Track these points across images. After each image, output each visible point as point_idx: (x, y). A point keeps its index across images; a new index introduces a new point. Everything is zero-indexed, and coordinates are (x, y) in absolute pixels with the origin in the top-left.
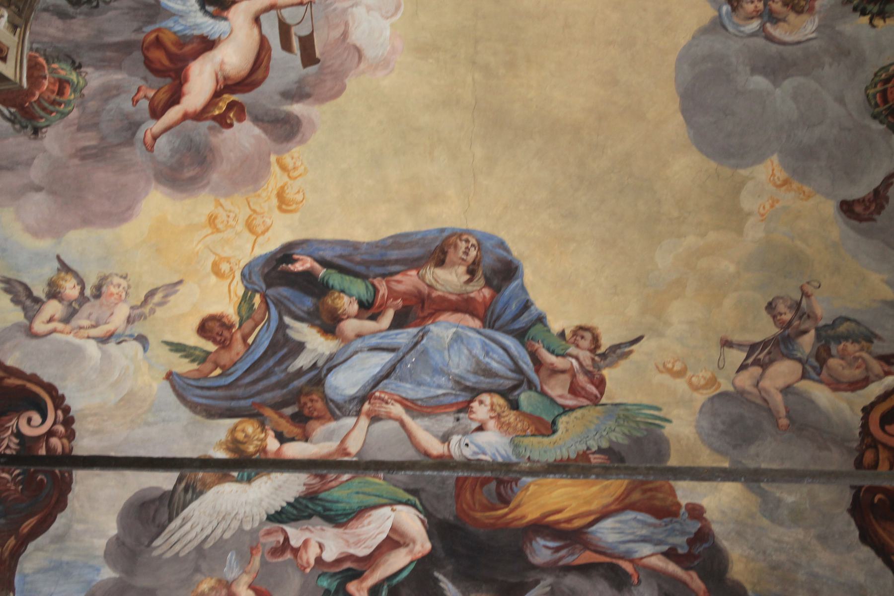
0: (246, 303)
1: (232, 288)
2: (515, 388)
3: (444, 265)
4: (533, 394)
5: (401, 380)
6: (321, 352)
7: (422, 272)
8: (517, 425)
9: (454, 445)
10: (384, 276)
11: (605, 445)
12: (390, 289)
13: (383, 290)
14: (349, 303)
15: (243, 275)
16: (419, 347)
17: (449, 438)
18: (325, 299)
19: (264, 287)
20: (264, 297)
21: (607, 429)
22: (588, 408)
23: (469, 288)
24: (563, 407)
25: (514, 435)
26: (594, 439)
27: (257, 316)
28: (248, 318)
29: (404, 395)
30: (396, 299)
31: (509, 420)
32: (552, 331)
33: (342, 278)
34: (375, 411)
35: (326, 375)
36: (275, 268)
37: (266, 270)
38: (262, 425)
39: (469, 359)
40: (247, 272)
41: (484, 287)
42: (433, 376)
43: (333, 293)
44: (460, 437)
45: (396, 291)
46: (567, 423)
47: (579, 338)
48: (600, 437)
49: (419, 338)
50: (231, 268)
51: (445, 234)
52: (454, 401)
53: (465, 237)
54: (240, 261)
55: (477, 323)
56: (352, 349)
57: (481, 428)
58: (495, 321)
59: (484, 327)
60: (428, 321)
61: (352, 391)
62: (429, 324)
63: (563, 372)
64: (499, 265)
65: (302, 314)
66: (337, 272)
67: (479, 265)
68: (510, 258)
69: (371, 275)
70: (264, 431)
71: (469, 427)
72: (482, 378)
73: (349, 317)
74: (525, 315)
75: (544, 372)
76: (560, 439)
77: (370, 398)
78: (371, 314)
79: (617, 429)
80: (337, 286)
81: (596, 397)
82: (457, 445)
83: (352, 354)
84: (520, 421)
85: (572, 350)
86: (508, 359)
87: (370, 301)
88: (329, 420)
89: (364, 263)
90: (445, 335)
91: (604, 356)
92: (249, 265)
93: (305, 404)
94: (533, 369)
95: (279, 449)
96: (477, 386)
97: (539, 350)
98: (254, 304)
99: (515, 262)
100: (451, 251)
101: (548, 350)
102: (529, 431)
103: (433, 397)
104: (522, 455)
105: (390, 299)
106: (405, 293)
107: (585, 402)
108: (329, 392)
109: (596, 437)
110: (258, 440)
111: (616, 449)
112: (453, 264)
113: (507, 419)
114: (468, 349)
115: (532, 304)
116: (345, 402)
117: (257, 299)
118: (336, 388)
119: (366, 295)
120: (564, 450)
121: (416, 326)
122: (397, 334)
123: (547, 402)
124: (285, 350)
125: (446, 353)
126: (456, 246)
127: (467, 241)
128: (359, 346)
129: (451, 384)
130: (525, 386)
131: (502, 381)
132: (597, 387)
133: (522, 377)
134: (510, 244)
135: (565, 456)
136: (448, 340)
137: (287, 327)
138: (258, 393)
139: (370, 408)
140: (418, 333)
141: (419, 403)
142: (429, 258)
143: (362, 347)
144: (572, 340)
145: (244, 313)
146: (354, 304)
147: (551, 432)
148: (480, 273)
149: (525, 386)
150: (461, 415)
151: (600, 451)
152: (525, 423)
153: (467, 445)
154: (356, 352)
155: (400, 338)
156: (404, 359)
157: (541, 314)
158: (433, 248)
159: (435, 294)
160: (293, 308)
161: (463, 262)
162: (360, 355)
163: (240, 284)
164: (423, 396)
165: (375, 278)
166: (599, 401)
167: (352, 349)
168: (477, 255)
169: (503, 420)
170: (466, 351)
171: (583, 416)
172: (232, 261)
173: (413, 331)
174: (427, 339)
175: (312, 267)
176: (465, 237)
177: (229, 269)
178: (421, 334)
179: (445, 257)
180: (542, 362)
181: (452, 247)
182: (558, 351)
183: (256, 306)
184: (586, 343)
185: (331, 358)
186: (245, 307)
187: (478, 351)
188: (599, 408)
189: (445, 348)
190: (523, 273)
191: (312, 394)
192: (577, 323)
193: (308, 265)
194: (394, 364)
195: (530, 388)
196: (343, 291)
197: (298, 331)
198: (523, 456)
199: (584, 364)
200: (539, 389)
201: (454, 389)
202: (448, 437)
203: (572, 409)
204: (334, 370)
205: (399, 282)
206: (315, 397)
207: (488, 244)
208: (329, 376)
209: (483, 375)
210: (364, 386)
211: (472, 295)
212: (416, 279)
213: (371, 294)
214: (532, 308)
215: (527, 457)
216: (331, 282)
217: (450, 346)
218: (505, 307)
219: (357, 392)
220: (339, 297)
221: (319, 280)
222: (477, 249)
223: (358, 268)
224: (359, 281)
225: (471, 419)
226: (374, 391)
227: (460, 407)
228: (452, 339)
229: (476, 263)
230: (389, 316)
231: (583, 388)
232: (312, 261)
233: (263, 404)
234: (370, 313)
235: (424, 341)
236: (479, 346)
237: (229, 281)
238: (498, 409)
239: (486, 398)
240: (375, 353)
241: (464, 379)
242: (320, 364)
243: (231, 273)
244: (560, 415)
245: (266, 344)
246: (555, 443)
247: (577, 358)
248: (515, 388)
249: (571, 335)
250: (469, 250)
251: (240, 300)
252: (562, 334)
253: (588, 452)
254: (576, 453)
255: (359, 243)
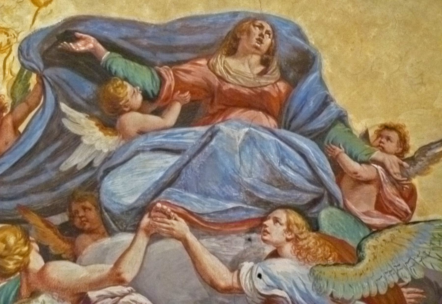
0: (21, 83)
1: (7, 63)
2: (315, 202)
3: (237, 54)
4: (334, 210)
5: (186, 189)
6: (99, 149)
7: (213, 61)
8: (317, 250)
9: (246, 273)
10: (171, 64)
11: (419, 275)
12: (177, 79)
13: (170, 81)
14: (132, 93)
15: (20, 50)
16: (207, 149)
17: (240, 265)
18: (108, 85)
19: (41, 65)
20: (41, 77)
21: (421, 255)
22: (398, 227)
23: (263, 81)
24: (369, 226)
25: (314, 264)
26: (407, 269)
27: (32, 100)
28: (21, 101)
29: (189, 208)
30: (183, 92)
31: (308, 243)
32: (354, 132)
33: (125, 62)
34: (156, 226)
35: (102, 178)
36: (55, 44)
37: (46, 47)
38: (26, 234)
39: (262, 166)
40: (25, 47)
41: (279, 81)
42: (223, 185)
43: (115, 80)
44: (252, 264)
45: (183, 82)
46: (375, 247)
47: (384, 140)
48: (414, 265)
49: (207, 139)
50: (8, 40)
51: (239, 19)
52: (246, 218)
53: (258, 23)
54: (18, 34)
55: (271, 122)
56: (133, 148)
57: (275, 254)
58: (291, 121)
59: (279, 127)
60: (218, 119)
61: (130, 200)
62: (219, 123)
63: (368, 182)
64: (295, 55)
65: (80, 102)
66: (121, 56)
67: (273, 55)
68: (306, 47)
69: (158, 62)
70: (27, 244)
71: (262, 251)
72: (277, 190)
73: (131, 110)
74: (324, 113)
75: (346, 183)
76: (367, 269)
77: (150, 211)
78: (156, 107)
79: (433, 253)
80: (121, 73)
81: (406, 212)
82: (249, 275)
83: (133, 154)
84: (320, 246)
85: (377, 155)
86: (309, 172)
87: (156, 92)
88: (103, 236)
89: (153, 49)
90: (237, 136)
91: (412, 160)
92: (27, 39)
93: (77, 212)
94: (335, 180)
95: (43, 269)
96: (271, 199)
97: (340, 156)
98: (29, 86)
99: (313, 51)
100: (244, 37)
101: (350, 156)
102: (331, 258)
103: (221, 212)
104: (323, 291)
105: (177, 91)
106: (193, 86)
107: (394, 220)
108: (105, 199)
109: (410, 264)
110: (19, 254)
111: (433, 279)
112: (246, 53)
113: (305, 242)
114: (262, 154)
115: (332, 100)
116: (122, 213)
117: (33, 79)
118: (113, 194)
119: (151, 84)
120: (372, 283)
121: (204, 124)
122: (183, 133)
123: (351, 221)
124: (59, 144)
125: (237, 156)
126: (249, 33)
127: (261, 27)
128: (141, 145)
129: (242, 196)
130: (325, 201)
131: (299, 194)
132: (407, 200)
133: (321, 190)
134: (306, 31)
135: (374, 292)
136: (239, 142)
137: (64, 115)
138: (25, 194)
139: (149, 222)
140: (207, 133)
141: (206, 218)
142: (221, 45)
143: (144, 146)
144: (377, 143)
145: (18, 96)
146: (138, 95)
147: (356, 261)
148: (274, 65)
149: (325, 201)
150: (254, 236)
151: (415, 282)
152: (327, 248)
153: (260, 276)
154: (137, 153)
155: (187, 138)
156: (190, 164)
157: (342, 112)
158: (225, 34)
159: (226, 87)
160: (72, 94)
161: (257, 51)
162: (141, 156)
163: (17, 59)
164: (210, 211)
165: (161, 66)
166: (410, 219)
167: (133, 148)
168: (272, 43)
169: (301, 243)
170: (259, 156)
171: (393, 238)
172: (11, 32)
173: (202, 129)
174: (216, 140)
175: (95, 48)
176: (258, 23)
177: (6, 42)
178: (209, 134)
179: (238, 45)
180: (345, 171)
181: (245, 33)
182: (360, 158)
183: (32, 87)
184: (392, 146)
185: (109, 157)
186: (20, 86)
187: (274, 158)
188: (410, 227)
189: (236, 151)
190: (321, 64)
191: (85, 200)
192: (382, 121)
193: (91, 45)
194: (180, 169)
195: (331, 204)
196: (126, 79)
197: (74, 122)
198: (325, 292)
199: (391, 171)
200: (342, 205)
201: (245, 203)
202: (239, 263)
203: (379, 230)
204: (112, 172)
205: (187, 72)
206: (88, 204)
207: (284, 31)
208: (106, 179)
209: (278, 187)
210: (144, 194)
211: (266, 89)
212: (206, 69)
213: (156, 83)
214: (332, 104)
215: (330, 293)
216: (114, 68)
217: (242, 149)
218: (303, 103)
219: (137, 201)
220: (122, 86)
221: (101, 64)
222: (271, 36)
223: (146, 54)
224: (144, 68)
225: (265, 241)
226: (155, 201)
227: (252, 225)
228: (244, 140)
229: (271, 51)
230: (177, 108)
231: (391, 203)
232: (96, 41)
233: (25, 209)
234: (154, 107)
235: (213, 143)
236: (273, 150)
237: (5, 55)
238: (295, 229)
239: (281, 215)
240: (157, 154)
241: (257, 190)
242: (97, 163)
243: (8, 46)
244: (365, 238)
245: (39, 134)
246: (361, 274)
247: (383, 165)
248: (315, 202)
249: (375, 138)
250: (263, 37)
251: (14, 78)
252: (365, 136)
253: (401, 284)
254: (387, 286)
255: (146, 25)
